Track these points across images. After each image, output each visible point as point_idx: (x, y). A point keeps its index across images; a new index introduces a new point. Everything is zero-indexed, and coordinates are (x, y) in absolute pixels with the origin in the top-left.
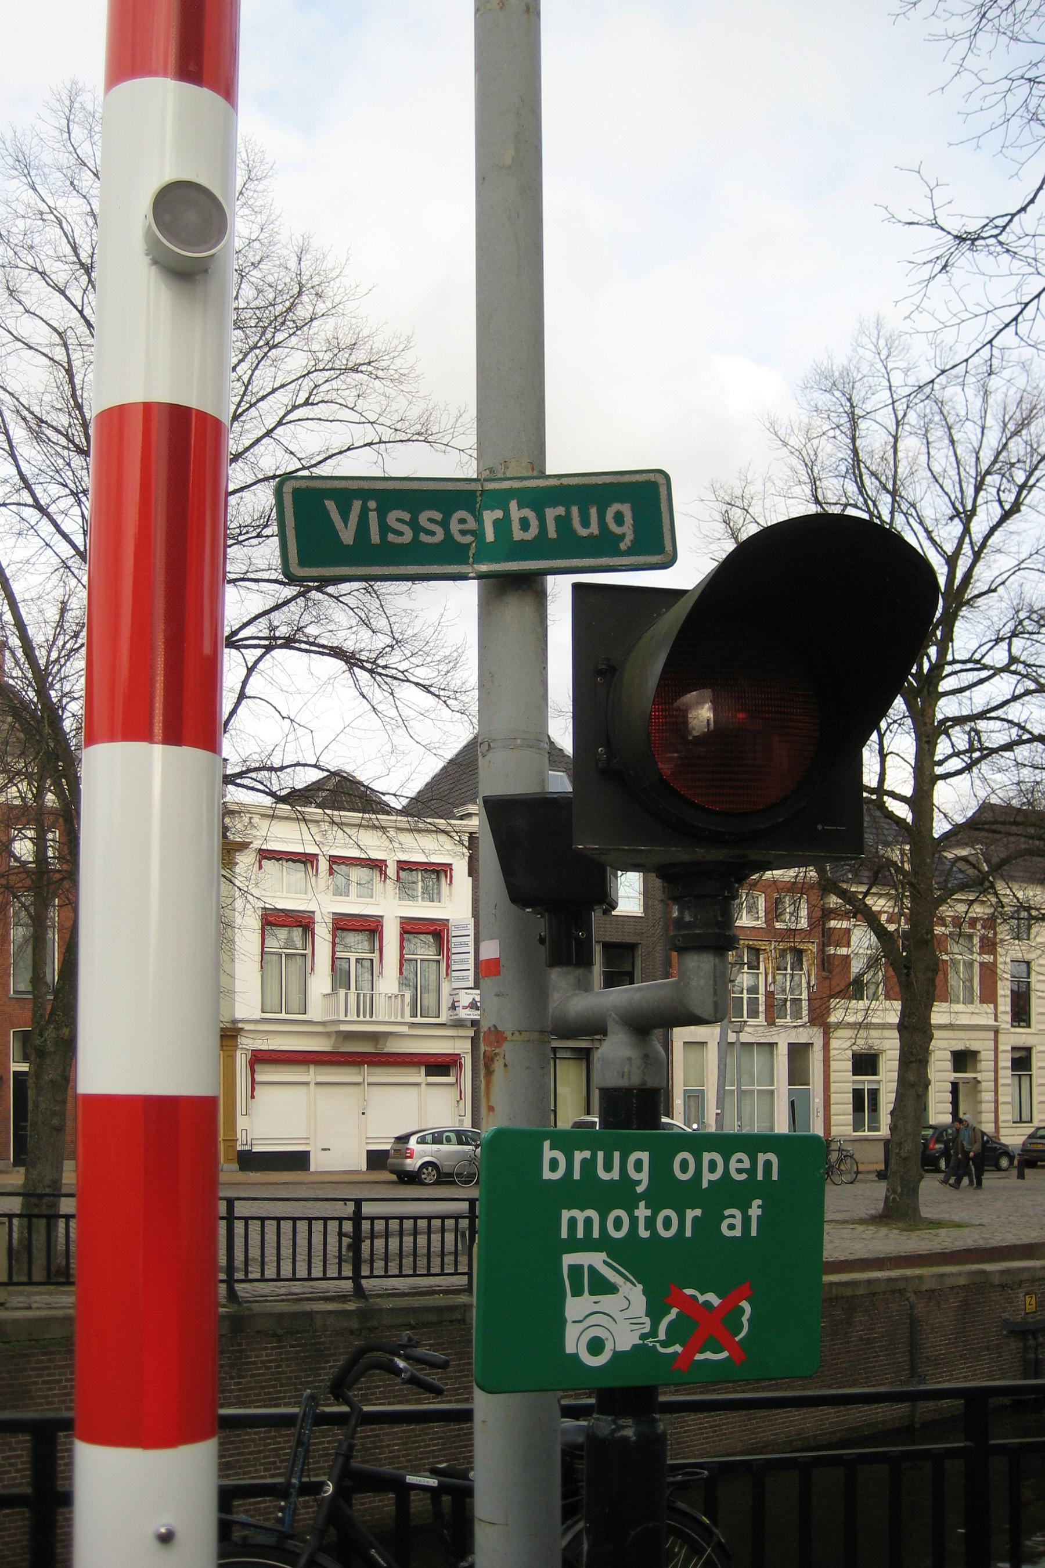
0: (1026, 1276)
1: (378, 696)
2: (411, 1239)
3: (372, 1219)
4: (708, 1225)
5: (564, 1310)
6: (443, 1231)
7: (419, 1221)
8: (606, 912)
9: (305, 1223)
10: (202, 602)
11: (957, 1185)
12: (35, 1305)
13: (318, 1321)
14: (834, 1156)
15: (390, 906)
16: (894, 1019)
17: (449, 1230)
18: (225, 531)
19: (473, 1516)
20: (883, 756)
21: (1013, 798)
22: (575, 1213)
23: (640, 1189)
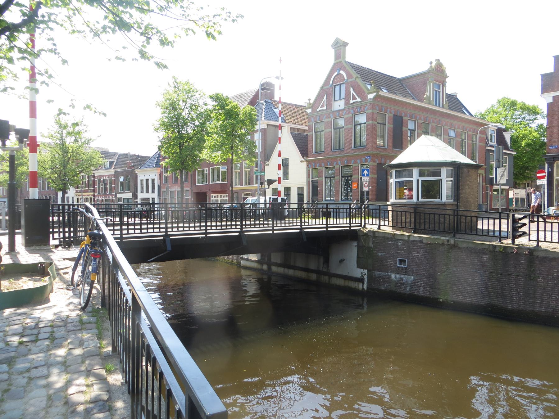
0: (456, 192)
1: (168, 14)
2: (448, 211)
3: (330, 209)
4: (72, 232)
5: (554, 63)
6: (376, 213)
7: (473, 218)
8: (543, 144)
9: (433, 215)
10: (460, 117)
11: (156, 130)
12: (499, 170)
13: (376, 233)
14: (117, 28)
15: (89, 197)
16: (356, 244)
17: (555, 232)
18: (491, 218)
19: (26, 236)
20: (508, 231)
21: (211, 111)
22: (217, 182)
23: (509, 378)
